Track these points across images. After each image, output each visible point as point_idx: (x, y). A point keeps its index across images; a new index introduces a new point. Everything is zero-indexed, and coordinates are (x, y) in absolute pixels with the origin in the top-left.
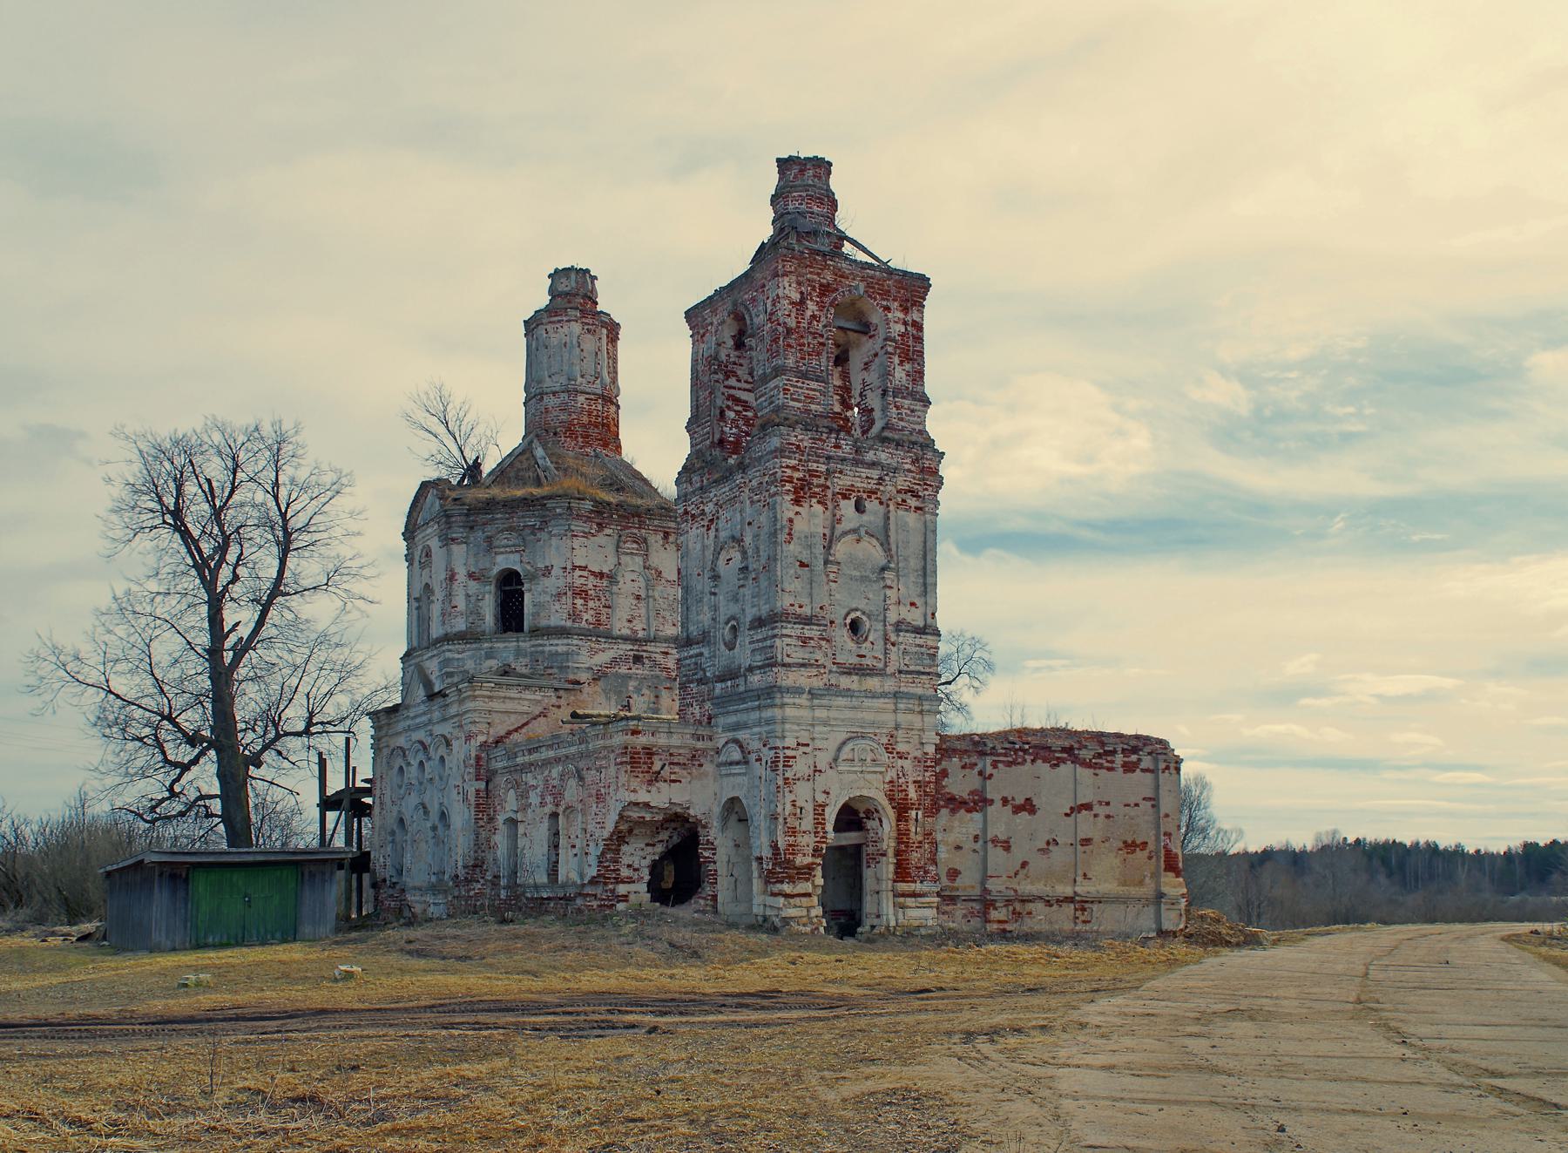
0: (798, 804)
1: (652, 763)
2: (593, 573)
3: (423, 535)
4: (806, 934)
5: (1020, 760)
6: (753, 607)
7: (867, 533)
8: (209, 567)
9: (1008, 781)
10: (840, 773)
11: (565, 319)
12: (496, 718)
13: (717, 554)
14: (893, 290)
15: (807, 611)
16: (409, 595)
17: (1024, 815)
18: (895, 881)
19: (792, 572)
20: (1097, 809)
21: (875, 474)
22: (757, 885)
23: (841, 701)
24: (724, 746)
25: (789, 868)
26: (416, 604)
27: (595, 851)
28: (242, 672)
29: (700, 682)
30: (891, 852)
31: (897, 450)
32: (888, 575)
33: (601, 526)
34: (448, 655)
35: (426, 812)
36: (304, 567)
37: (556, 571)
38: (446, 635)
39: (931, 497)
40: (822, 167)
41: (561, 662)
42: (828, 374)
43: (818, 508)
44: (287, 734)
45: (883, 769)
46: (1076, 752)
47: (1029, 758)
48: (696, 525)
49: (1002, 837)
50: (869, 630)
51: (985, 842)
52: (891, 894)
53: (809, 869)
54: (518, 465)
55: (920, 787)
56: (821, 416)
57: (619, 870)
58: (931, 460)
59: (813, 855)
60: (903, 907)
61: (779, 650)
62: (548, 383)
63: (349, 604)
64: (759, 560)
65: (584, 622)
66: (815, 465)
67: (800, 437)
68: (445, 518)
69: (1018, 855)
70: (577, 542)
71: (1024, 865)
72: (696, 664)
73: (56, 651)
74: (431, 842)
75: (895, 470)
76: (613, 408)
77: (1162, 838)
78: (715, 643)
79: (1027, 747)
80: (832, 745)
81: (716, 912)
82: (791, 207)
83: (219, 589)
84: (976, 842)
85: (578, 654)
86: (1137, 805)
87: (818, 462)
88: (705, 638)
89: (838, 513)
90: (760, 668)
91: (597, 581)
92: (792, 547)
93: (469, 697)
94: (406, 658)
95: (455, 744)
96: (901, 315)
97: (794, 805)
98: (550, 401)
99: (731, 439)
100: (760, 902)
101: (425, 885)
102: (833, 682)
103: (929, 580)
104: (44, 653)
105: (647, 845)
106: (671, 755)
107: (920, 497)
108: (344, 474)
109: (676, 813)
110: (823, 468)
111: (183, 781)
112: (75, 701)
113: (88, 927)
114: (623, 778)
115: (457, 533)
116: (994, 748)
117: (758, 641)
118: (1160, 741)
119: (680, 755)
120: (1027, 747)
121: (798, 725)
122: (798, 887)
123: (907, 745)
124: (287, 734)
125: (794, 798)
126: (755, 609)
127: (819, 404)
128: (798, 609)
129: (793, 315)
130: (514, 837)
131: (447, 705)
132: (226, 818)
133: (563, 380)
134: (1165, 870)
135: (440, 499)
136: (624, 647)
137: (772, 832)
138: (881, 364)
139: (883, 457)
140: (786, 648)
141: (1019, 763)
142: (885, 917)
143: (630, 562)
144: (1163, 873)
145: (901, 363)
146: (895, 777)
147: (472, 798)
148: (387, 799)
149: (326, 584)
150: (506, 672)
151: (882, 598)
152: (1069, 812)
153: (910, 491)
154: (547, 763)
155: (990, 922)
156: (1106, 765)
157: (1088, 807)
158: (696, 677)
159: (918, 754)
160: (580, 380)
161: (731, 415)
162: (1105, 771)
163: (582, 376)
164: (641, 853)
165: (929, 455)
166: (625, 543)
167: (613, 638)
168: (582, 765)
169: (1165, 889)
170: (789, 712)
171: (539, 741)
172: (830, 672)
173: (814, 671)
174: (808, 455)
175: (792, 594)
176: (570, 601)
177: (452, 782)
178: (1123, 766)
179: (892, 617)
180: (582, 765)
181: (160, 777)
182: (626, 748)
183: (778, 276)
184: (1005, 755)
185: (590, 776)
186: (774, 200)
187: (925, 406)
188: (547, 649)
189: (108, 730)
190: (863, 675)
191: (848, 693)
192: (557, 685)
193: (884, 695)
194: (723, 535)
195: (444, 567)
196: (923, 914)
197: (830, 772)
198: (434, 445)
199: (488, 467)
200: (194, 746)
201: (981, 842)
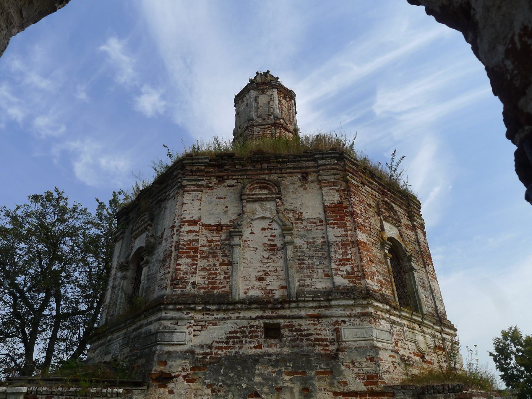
2: (208, 227)
5: (275, 253)
8: (503, 364)
143: (259, 209)
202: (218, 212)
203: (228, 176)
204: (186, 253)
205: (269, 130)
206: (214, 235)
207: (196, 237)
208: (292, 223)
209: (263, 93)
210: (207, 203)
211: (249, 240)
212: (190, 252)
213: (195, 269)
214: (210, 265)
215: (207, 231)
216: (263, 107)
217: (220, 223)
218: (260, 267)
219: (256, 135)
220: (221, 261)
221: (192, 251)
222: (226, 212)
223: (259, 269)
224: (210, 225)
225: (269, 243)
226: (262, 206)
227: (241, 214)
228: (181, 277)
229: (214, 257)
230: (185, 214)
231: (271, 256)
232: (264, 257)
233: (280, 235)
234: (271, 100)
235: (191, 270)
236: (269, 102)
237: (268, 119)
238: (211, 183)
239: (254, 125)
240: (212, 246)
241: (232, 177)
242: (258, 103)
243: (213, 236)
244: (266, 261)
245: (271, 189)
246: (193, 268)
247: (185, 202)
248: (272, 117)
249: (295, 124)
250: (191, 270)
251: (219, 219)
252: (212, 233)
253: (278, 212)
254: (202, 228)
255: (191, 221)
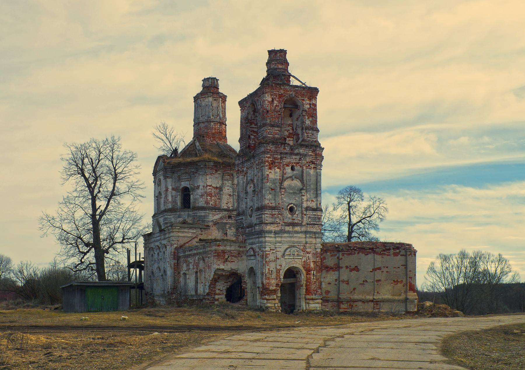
0: (270, 269)
1: (225, 256)
2: (214, 187)
3: (159, 174)
4: (273, 312)
5: (353, 253)
6: (257, 204)
7: (295, 177)
9: (347, 260)
10: (286, 259)
11: (207, 96)
12: (180, 239)
13: (247, 184)
14: (305, 94)
15: (274, 205)
16: (155, 195)
17: (354, 272)
18: (305, 295)
19: (268, 192)
20: (383, 269)
21: (298, 157)
22: (258, 296)
23: (286, 235)
24: (249, 250)
25: (267, 290)
26: (156, 198)
27: (208, 284)
28: (102, 222)
29: (242, 228)
30: (304, 285)
31: (306, 148)
32: (303, 191)
33: (216, 171)
34: (166, 216)
35: (160, 270)
36: (121, 186)
37: (201, 187)
38: (165, 209)
39: (319, 164)
40: (283, 52)
41: (202, 219)
42: (282, 125)
43: (278, 170)
44: (116, 243)
45: (301, 257)
46: (375, 250)
47: (356, 252)
48: (241, 175)
49: (346, 280)
50: (296, 210)
51: (339, 281)
52: (304, 299)
53: (275, 291)
54: (190, 149)
55: (315, 263)
56: (279, 139)
57: (215, 291)
58: (319, 151)
59: (276, 286)
60: (308, 303)
61: (264, 218)
62: (201, 119)
63: (136, 198)
64: (258, 188)
65: (210, 205)
66: (276, 156)
67: (271, 147)
68: (165, 169)
69: (352, 285)
70: (208, 177)
71: (354, 289)
72: (241, 222)
73: (47, 216)
74: (161, 280)
75: (306, 155)
76: (224, 126)
77: (408, 279)
78: (246, 215)
79: (355, 248)
80: (283, 250)
81: (247, 305)
82: (272, 67)
83: (95, 195)
84: (336, 281)
85: (209, 216)
86: (399, 268)
87: (277, 155)
88: (243, 213)
89: (285, 172)
90: (258, 224)
91: (215, 190)
92: (268, 184)
93: (171, 231)
94: (154, 217)
95: (168, 247)
96: (308, 102)
97: (269, 270)
98: (202, 125)
99: (253, 145)
100: (259, 302)
101: (159, 294)
102: (283, 228)
103: (319, 192)
104: (44, 217)
105: (225, 282)
106: (231, 253)
107: (315, 164)
108: (133, 154)
109: (234, 272)
110: (279, 157)
111: (85, 257)
112: (53, 232)
113: (57, 306)
114: (215, 261)
115: (169, 174)
116: (342, 249)
117: (258, 215)
118: (408, 245)
119: (234, 253)
120: (355, 248)
121: (271, 243)
122: (271, 297)
123: (310, 249)
124: (116, 243)
125: (269, 267)
126: (257, 204)
127: (278, 135)
128: (270, 205)
129: (269, 106)
130: (185, 279)
131: (165, 234)
132: (98, 271)
133: (206, 118)
134: (409, 290)
135: (163, 163)
136: (225, 213)
137: (262, 279)
138: (302, 119)
139: (301, 151)
140: (266, 218)
141: (352, 254)
142: (302, 307)
144: (408, 291)
145: (308, 118)
146: (306, 260)
147: (173, 266)
148: (148, 265)
149: (128, 191)
150: (184, 222)
151: (301, 199)
152: (372, 270)
153: (311, 162)
154: (195, 255)
155: (341, 308)
156: (387, 254)
157: (379, 269)
158: (241, 226)
159: (314, 252)
160: (212, 117)
161: (253, 137)
162: (386, 256)
163: (213, 116)
164: (223, 285)
165: (318, 149)
166: (225, 176)
167: (221, 210)
168: (204, 256)
169: (409, 297)
170: (267, 239)
171: (192, 247)
172: (282, 225)
173: (276, 225)
174: (274, 153)
175: (268, 199)
176: (205, 197)
177: (167, 260)
178: (393, 254)
179: (305, 205)
180: (204, 256)
181: (78, 257)
182: (216, 251)
183: (264, 93)
184: (347, 251)
185: (207, 259)
186: (267, 64)
187: (317, 132)
188: (198, 214)
189: (62, 242)
190: (294, 226)
191: (288, 232)
192: (201, 227)
193: (301, 232)
194: (249, 178)
195: (165, 186)
196: (316, 306)
197: (282, 259)
198: (162, 144)
199: (180, 150)
200: (87, 247)
201: (338, 281)
226: (228, 182)
229: (216, 197)
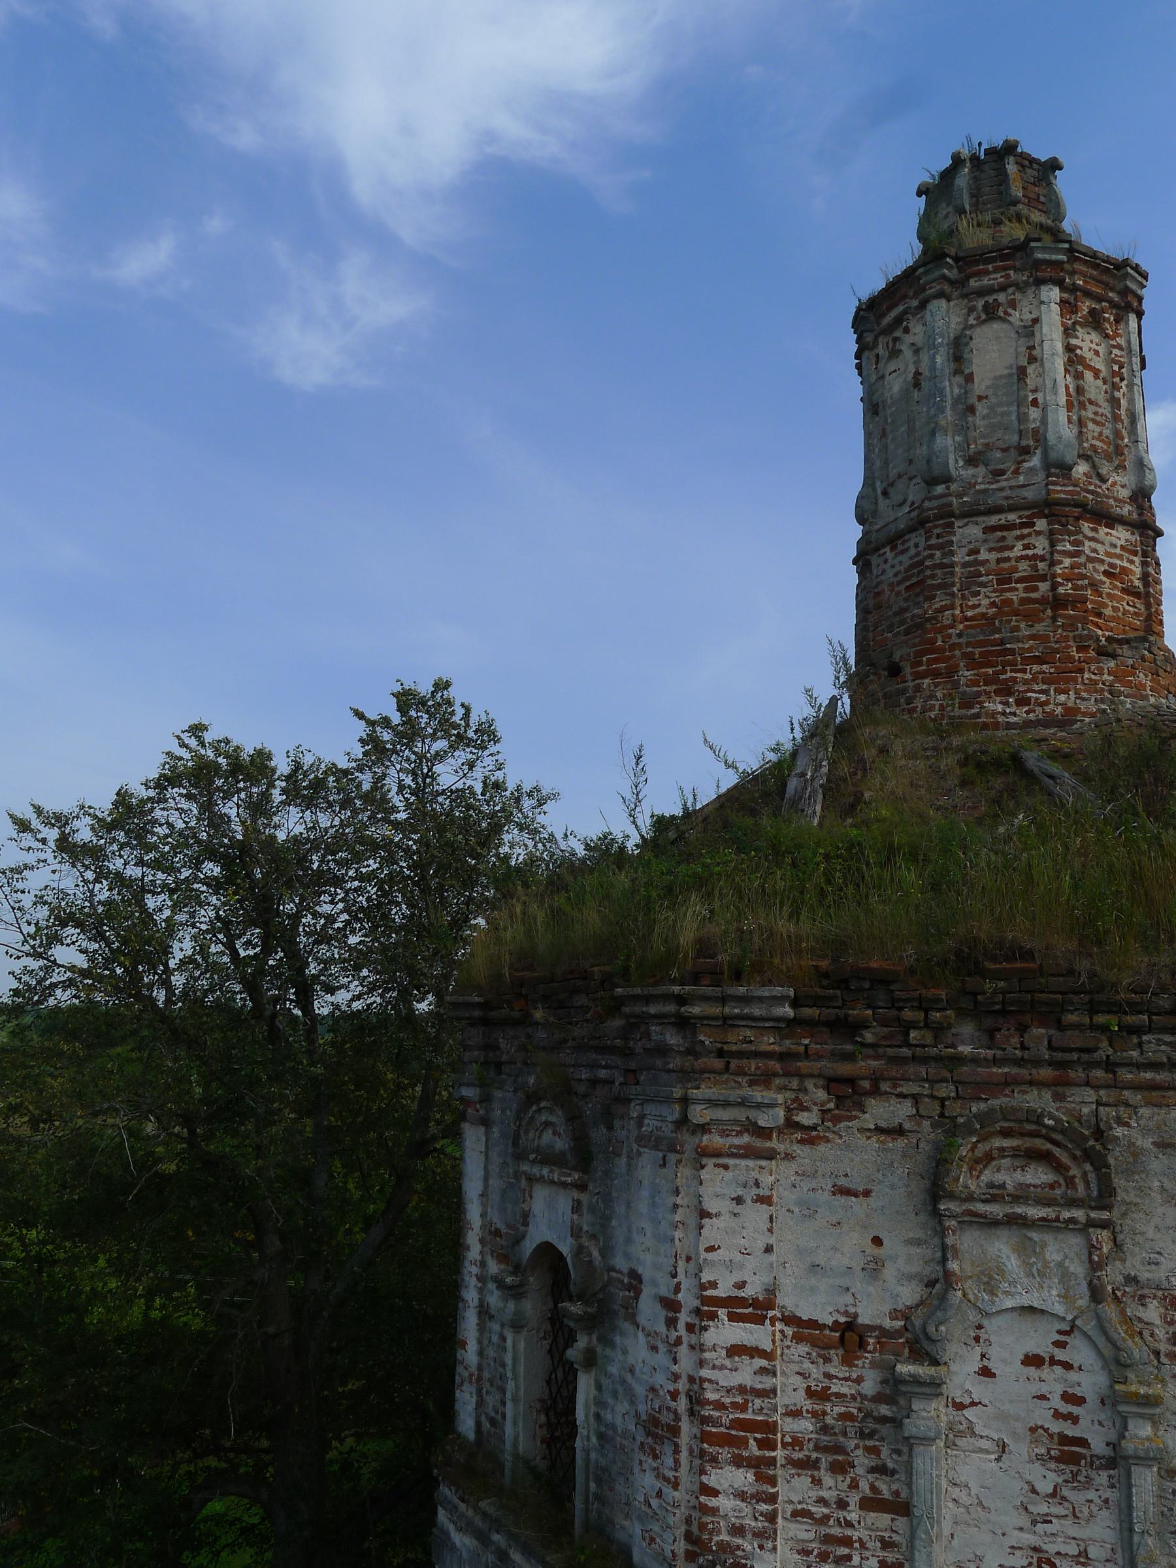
143: (1013, 1263)
202: (846, 1262)
203: (876, 1079)
204: (730, 1446)
205: (1022, 537)
206: (833, 1371)
207: (764, 1378)
208: (1157, 1353)
209: (991, 314)
210: (796, 1210)
211: (973, 1404)
212: (744, 1443)
213: (772, 1518)
214: (822, 1501)
215: (803, 1349)
216: (993, 400)
217: (856, 1315)
218: (1021, 1529)
219: (965, 565)
220: (867, 1491)
221: (755, 1439)
222: (874, 1268)
223: (1016, 1538)
224: (813, 1324)
225: (1056, 1427)
226: (1025, 1250)
227: (937, 1281)
228: (720, 1544)
229: (838, 1468)
230: (712, 1264)
231: (1065, 1492)
232: (1034, 1491)
233: (1103, 1402)
234: (1032, 359)
235: (756, 1519)
236: (1022, 372)
237: (1016, 472)
238: (806, 1109)
239: (952, 515)
240: (829, 1420)
241: (895, 1086)
242: (969, 378)
243: (828, 1376)
244: (1043, 1508)
245: (1067, 1169)
246: (762, 1514)
247: (711, 1205)
248: (1035, 461)
249: (1141, 466)
250: (756, 1519)
251: (848, 1299)
252: (827, 1360)
253: (1096, 1294)
254: (782, 1332)
255: (741, 1302)
